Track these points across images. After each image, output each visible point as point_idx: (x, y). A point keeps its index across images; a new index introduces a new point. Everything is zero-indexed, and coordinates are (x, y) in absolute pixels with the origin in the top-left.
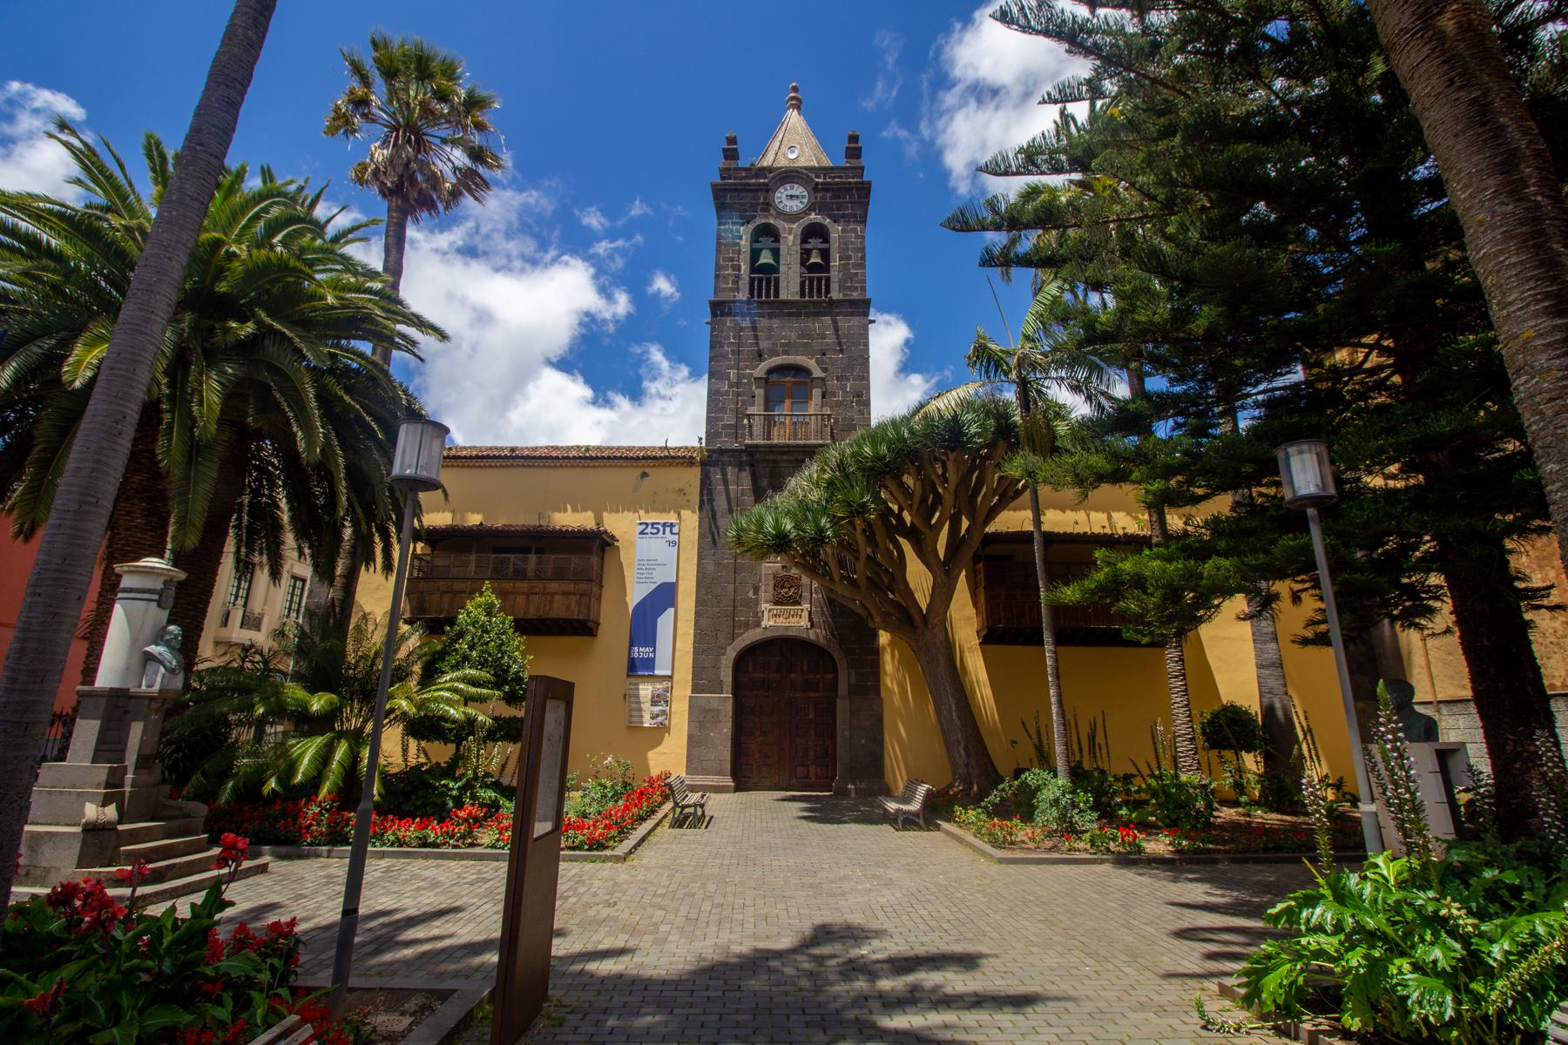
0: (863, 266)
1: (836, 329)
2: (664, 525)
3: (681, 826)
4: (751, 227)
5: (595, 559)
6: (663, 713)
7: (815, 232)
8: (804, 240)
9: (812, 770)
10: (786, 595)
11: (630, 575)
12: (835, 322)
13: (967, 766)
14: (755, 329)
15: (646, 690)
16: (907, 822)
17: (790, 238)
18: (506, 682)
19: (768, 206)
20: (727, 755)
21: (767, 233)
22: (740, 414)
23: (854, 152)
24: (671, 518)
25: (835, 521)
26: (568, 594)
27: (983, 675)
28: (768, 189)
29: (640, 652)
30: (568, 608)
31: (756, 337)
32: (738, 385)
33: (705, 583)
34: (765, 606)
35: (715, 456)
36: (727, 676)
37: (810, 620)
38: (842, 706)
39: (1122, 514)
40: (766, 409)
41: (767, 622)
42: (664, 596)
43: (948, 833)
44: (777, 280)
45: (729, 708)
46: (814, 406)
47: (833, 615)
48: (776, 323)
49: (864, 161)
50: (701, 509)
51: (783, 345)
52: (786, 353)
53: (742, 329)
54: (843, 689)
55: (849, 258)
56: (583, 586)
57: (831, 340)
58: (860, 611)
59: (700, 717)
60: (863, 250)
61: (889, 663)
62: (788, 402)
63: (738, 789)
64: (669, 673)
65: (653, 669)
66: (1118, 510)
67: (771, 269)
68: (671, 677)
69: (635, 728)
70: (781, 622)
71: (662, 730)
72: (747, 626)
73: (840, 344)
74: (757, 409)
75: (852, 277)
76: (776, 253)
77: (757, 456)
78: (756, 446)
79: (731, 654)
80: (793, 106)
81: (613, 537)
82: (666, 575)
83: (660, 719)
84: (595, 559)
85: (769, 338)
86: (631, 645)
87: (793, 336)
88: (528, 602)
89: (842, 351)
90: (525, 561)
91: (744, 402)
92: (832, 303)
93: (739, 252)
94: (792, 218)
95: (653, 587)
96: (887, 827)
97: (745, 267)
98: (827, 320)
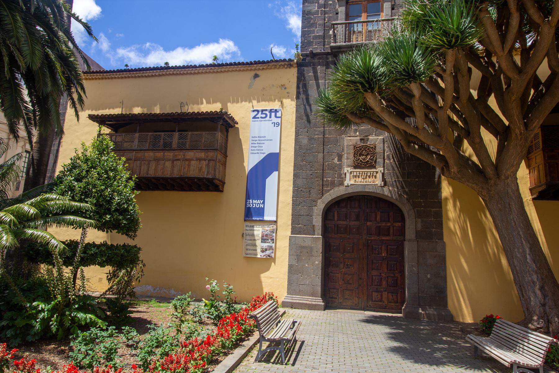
2: (271, 111)
3: (267, 361)
5: (219, 135)
6: (271, 248)
9: (385, 295)
10: (364, 158)
11: (246, 147)
15: (258, 231)
18: (108, 211)
20: (318, 282)
24: (276, 105)
26: (200, 160)
29: (255, 203)
30: (200, 170)
32: (325, 6)
33: (301, 153)
34: (347, 170)
35: (308, 60)
36: (318, 221)
37: (384, 179)
41: (349, 181)
42: (271, 163)
45: (319, 246)
50: (298, 98)
56: (211, 154)
59: (298, 253)
61: (452, 211)
63: (327, 307)
64: (275, 219)
65: (263, 215)
68: (276, 222)
69: (251, 259)
71: (270, 260)
72: (333, 185)
74: (341, 18)
79: (321, 205)
81: (232, 119)
83: (268, 252)
84: (219, 135)
86: (248, 197)
88: (173, 166)
90: (171, 137)
95: (263, 156)
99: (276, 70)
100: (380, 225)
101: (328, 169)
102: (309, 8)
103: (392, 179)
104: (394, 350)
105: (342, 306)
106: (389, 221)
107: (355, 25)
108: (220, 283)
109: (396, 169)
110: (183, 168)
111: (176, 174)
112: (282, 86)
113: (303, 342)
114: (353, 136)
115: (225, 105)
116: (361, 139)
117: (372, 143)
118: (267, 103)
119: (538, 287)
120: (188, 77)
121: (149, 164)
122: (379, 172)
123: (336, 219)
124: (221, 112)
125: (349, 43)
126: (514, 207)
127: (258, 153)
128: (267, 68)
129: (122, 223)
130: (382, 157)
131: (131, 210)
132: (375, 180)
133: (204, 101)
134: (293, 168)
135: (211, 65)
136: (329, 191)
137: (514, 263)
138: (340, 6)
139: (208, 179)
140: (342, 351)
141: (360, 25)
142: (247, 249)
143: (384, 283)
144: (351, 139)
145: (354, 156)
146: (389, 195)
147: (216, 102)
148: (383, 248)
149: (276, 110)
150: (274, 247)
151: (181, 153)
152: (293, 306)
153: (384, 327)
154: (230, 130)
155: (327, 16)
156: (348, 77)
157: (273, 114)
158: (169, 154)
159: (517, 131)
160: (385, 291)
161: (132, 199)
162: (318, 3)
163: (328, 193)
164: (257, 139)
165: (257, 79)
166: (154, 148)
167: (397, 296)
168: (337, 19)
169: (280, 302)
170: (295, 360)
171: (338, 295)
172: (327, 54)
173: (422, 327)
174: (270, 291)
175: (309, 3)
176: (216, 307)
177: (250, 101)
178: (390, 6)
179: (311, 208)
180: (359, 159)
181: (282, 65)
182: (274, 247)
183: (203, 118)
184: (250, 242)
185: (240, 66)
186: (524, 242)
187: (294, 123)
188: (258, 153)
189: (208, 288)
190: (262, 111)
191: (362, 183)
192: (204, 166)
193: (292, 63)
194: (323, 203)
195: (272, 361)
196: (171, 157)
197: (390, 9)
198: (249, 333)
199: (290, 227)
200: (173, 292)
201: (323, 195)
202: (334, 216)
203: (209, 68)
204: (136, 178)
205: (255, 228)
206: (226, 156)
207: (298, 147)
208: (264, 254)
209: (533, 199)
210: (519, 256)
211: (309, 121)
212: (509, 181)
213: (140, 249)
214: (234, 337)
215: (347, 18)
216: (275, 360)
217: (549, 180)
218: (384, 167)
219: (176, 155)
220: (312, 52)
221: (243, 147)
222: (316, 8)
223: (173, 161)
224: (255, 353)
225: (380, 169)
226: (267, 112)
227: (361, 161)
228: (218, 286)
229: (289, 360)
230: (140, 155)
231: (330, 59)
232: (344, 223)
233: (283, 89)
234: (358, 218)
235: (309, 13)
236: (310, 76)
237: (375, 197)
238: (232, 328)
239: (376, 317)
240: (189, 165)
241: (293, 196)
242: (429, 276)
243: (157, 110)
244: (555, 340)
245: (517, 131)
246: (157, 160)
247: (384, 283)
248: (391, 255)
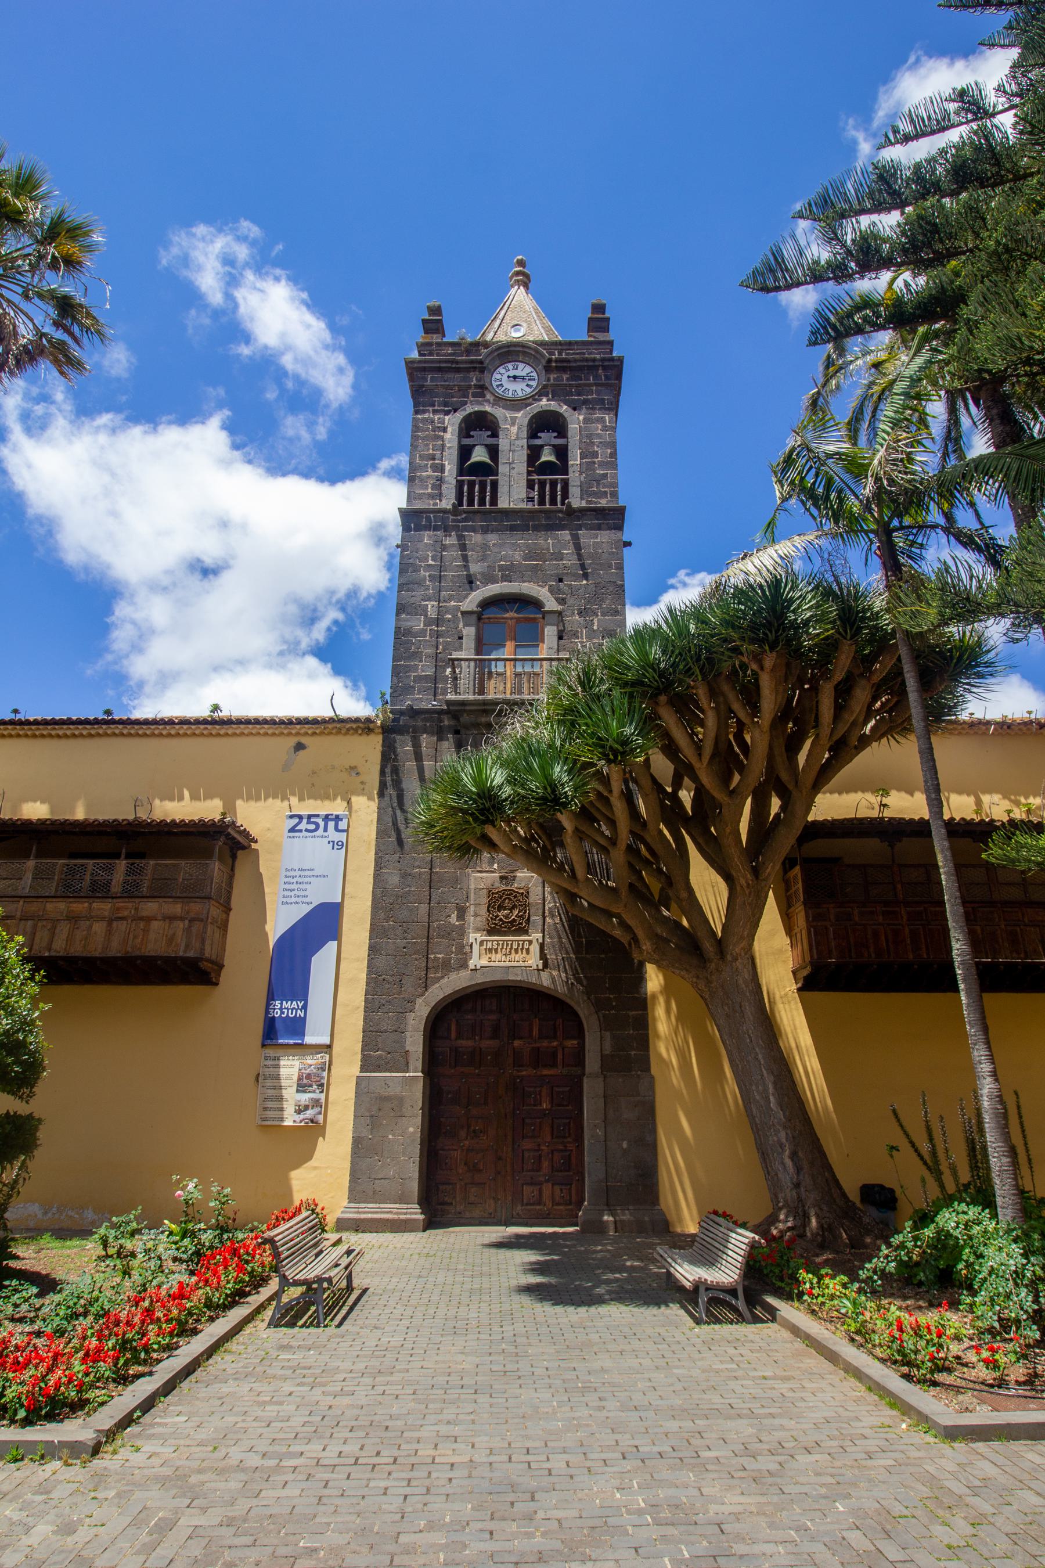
0: (614, 466)
1: (578, 547)
2: (327, 818)
3: (292, 1324)
4: (459, 416)
5: (216, 867)
6: (316, 1103)
7: (546, 424)
8: (533, 434)
9: (547, 1190)
10: (507, 916)
11: (271, 891)
12: (576, 538)
13: (797, 1185)
14: (463, 547)
15: (290, 1068)
16: (712, 1305)
17: (513, 430)
19: (482, 389)
20: (413, 1170)
21: (480, 424)
22: (441, 661)
23: (599, 320)
24: (337, 807)
25: (577, 768)
26: (171, 918)
27: (805, 1039)
28: (481, 368)
30: (171, 940)
31: (465, 558)
32: (438, 622)
33: (385, 904)
34: (474, 937)
35: (403, 720)
36: (415, 1043)
37: (543, 956)
38: (592, 1090)
39: (996, 798)
40: (478, 653)
41: (477, 960)
42: (322, 924)
43: (796, 1331)
44: (495, 485)
45: (416, 1095)
46: (548, 647)
47: (577, 949)
48: (492, 539)
49: (611, 336)
50: (381, 794)
51: (502, 568)
52: (507, 578)
53: (444, 548)
54: (592, 1063)
55: (595, 455)
56: (196, 907)
57: (570, 560)
58: (617, 933)
59: (372, 1108)
60: (613, 445)
61: (663, 1021)
62: (510, 645)
63: (430, 1224)
64: (326, 1040)
65: (302, 1034)
66: (990, 791)
67: (487, 470)
68: (329, 1047)
69: (271, 1127)
70: (498, 959)
71: (314, 1130)
72: (447, 967)
73: (583, 567)
74: (467, 651)
75: (599, 480)
76: (494, 451)
77: (465, 719)
78: (463, 703)
79: (423, 1008)
80: (518, 283)
81: (246, 834)
82: (320, 894)
83: (309, 1113)
84: (216, 867)
85: (484, 558)
86: (271, 997)
87: (518, 557)
88: (109, 932)
89: (585, 576)
90: (109, 869)
91: (446, 645)
92: (571, 512)
93: (443, 448)
94: (517, 404)
96: (675, 1312)
97: (450, 468)
98: (565, 535)
99: (340, 737)
100: (538, 1045)
101: (439, 936)
102: (409, 623)
103: (556, 955)
104: (528, 1290)
105: (462, 1221)
106: (555, 1037)
107: (493, 663)
108: (204, 1185)
109: (563, 935)
110: (131, 936)
111: (115, 950)
112: (352, 768)
113: (365, 1290)
114: (487, 872)
115: (230, 808)
116: (502, 878)
117: (522, 885)
118: (319, 802)
119: (787, 1153)
120: (153, 742)
121: (54, 928)
122: (535, 941)
123: (453, 1035)
124: (222, 820)
125: (481, 697)
126: (749, 1010)
127: (296, 903)
128: (322, 733)
129: (12, 1071)
130: (541, 911)
131: (31, 1044)
132: (528, 957)
133: (186, 794)
134: (368, 934)
135: (205, 722)
136: (438, 979)
137: (752, 1111)
138: (466, 625)
139: (185, 960)
140: (435, 1298)
141: (500, 664)
142: (265, 1109)
143: (545, 1164)
144: (483, 876)
145: (488, 911)
146: (552, 987)
147: (212, 798)
148: (545, 1091)
149: (337, 816)
150: (323, 1101)
151: (130, 905)
152: (358, 1226)
153: (529, 1252)
154: (240, 853)
155: (441, 640)
156: (452, 801)
157: (331, 825)
158: (102, 906)
159: (743, 881)
160: (547, 1181)
161: (33, 1021)
162: (426, 616)
163: (437, 985)
164: (297, 873)
165: (301, 753)
166: (68, 892)
167: (570, 1189)
168: (460, 649)
169: (331, 1220)
170: (345, 1318)
171: (455, 1197)
172: (440, 712)
173: (600, 1248)
174: (311, 1197)
175: (408, 614)
176: (193, 1234)
177: (284, 798)
178: (556, 633)
179: (402, 1015)
180: (497, 916)
181: (352, 728)
182: (323, 1101)
183: (182, 832)
184: (271, 1092)
185: (266, 726)
186: (765, 1072)
187: (374, 843)
188: (296, 903)
189: (180, 1196)
190: (310, 817)
191: (502, 964)
192: (179, 933)
193: (371, 726)
194: (427, 1004)
195: (300, 1323)
196: (106, 914)
197: (556, 639)
198: (259, 1281)
199: (359, 1057)
200: (90, 1215)
201: (426, 988)
202: (449, 1029)
203: (202, 727)
204: (44, 977)
205: (282, 1063)
206: (228, 909)
207: (379, 891)
208: (302, 1116)
209: (799, 990)
210: (757, 1097)
211: (400, 842)
212: (738, 964)
213: (40, 1121)
214: (230, 1286)
215: (479, 651)
216: (306, 1322)
217: (815, 957)
218: (543, 931)
219: (118, 909)
220: (411, 707)
221: (266, 890)
222: (422, 625)
223: (110, 922)
224: (268, 1313)
225: (536, 936)
226: (320, 821)
227: (501, 920)
228: (199, 1191)
229: (332, 1320)
230: (34, 907)
231: (446, 723)
232: (470, 1043)
233: (354, 774)
234: (495, 1034)
235: (408, 632)
236: (405, 753)
237: (528, 989)
238: (226, 1268)
239: (518, 1236)
240: (146, 931)
241: (367, 991)
242: (625, 1145)
243: (80, 814)
244: (757, 1237)
245: (743, 881)
246: (74, 919)
247: (545, 1164)
248: (559, 1105)
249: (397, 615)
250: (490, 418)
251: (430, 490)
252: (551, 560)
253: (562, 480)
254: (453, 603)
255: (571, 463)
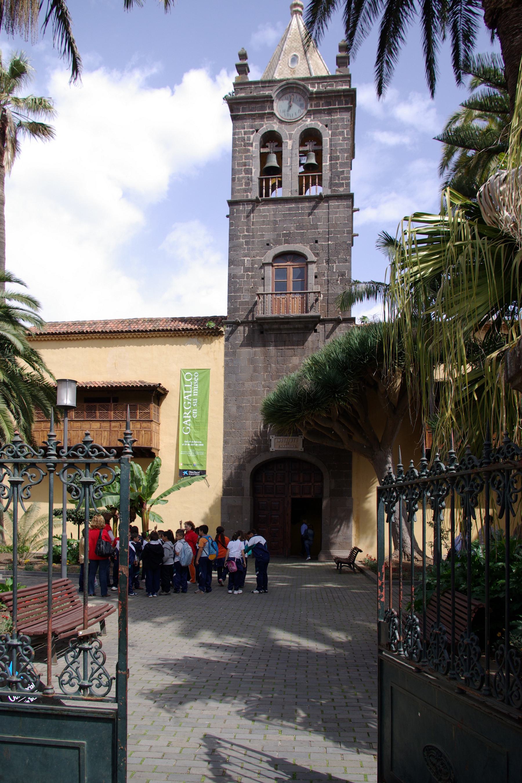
4: (260, 134)
7: (310, 137)
21: (272, 139)
51: (285, 235)
52: (287, 242)
54: (326, 491)
175: (234, 265)
203: (137, 334)
249: (229, 266)
250: (277, 134)
251: (244, 187)
252: (311, 229)
253: (318, 175)
254: (258, 258)
255: (324, 164)
